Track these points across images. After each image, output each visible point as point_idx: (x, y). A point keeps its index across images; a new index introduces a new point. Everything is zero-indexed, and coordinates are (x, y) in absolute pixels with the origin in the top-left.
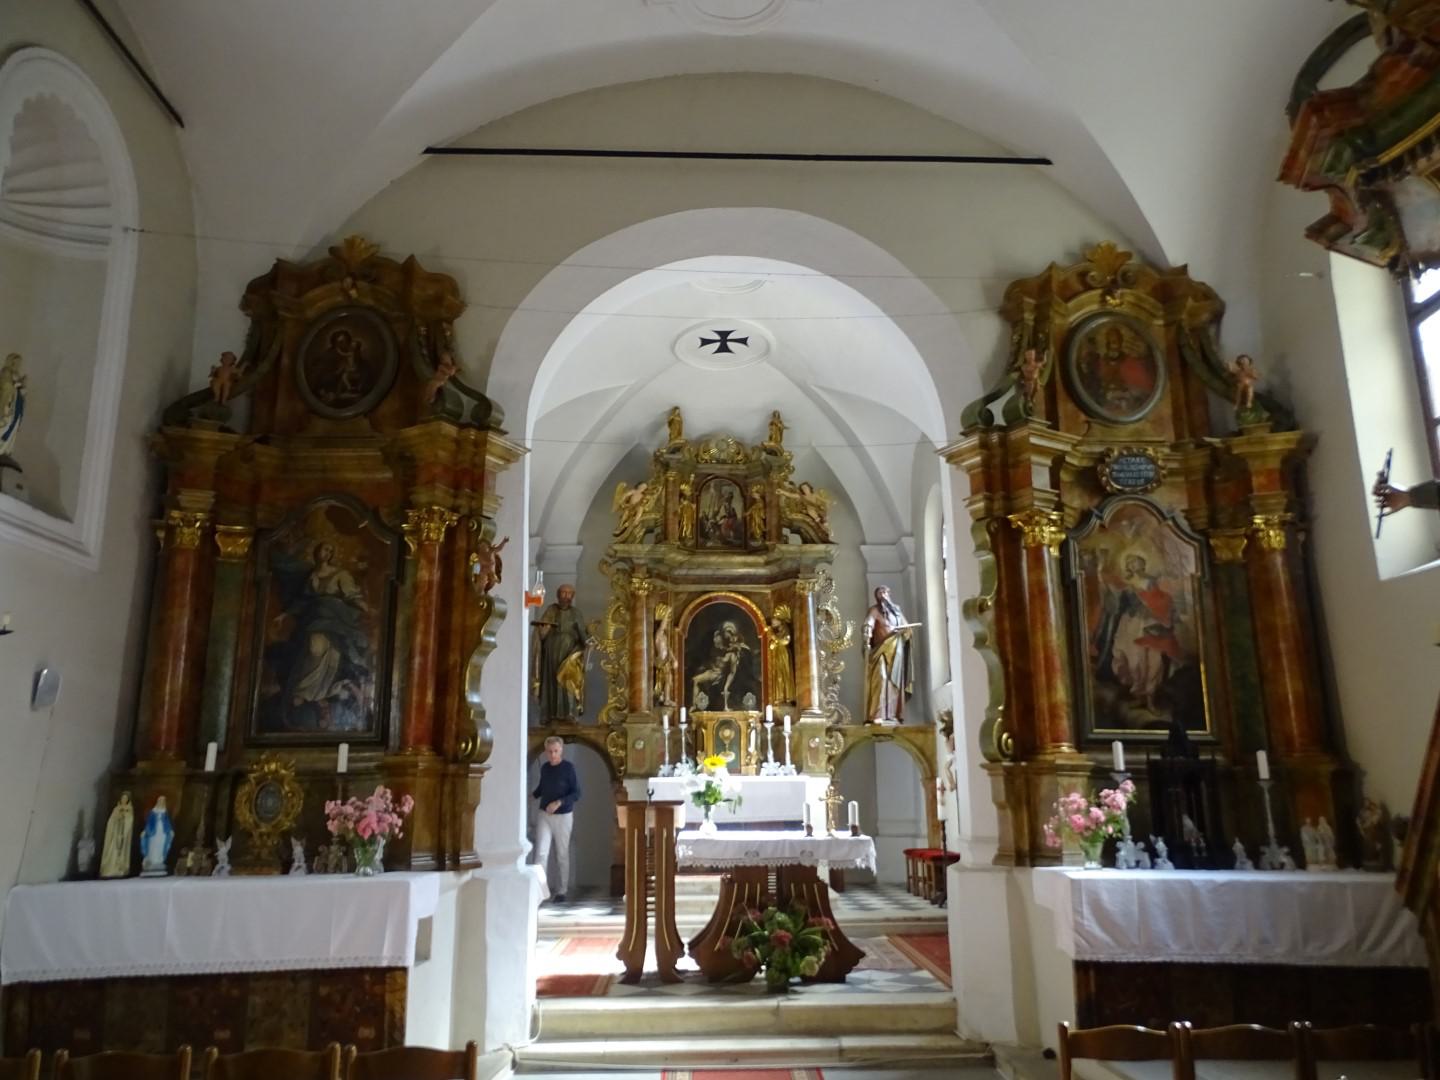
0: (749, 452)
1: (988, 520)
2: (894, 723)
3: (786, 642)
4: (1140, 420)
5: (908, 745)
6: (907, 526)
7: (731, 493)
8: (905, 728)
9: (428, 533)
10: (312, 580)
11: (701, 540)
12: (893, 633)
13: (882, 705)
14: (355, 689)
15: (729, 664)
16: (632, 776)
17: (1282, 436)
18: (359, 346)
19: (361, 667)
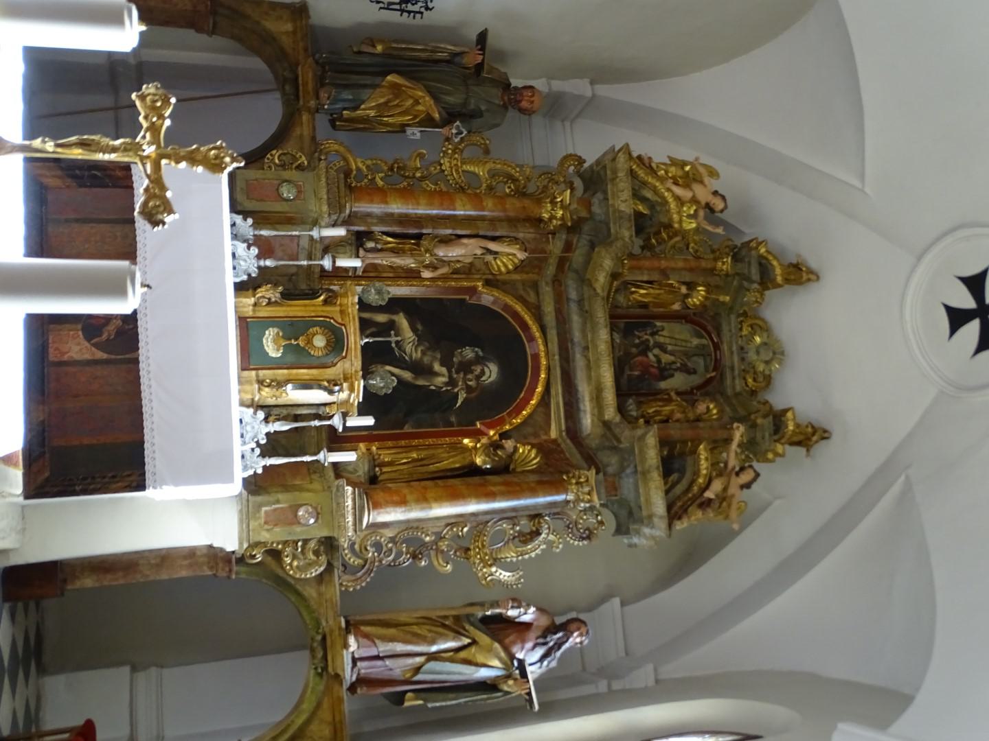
2: (349, 676)
3: (478, 461)
5: (307, 707)
6: (672, 670)
7: (695, 372)
8: (340, 700)
12: (512, 657)
13: (384, 648)
15: (429, 372)
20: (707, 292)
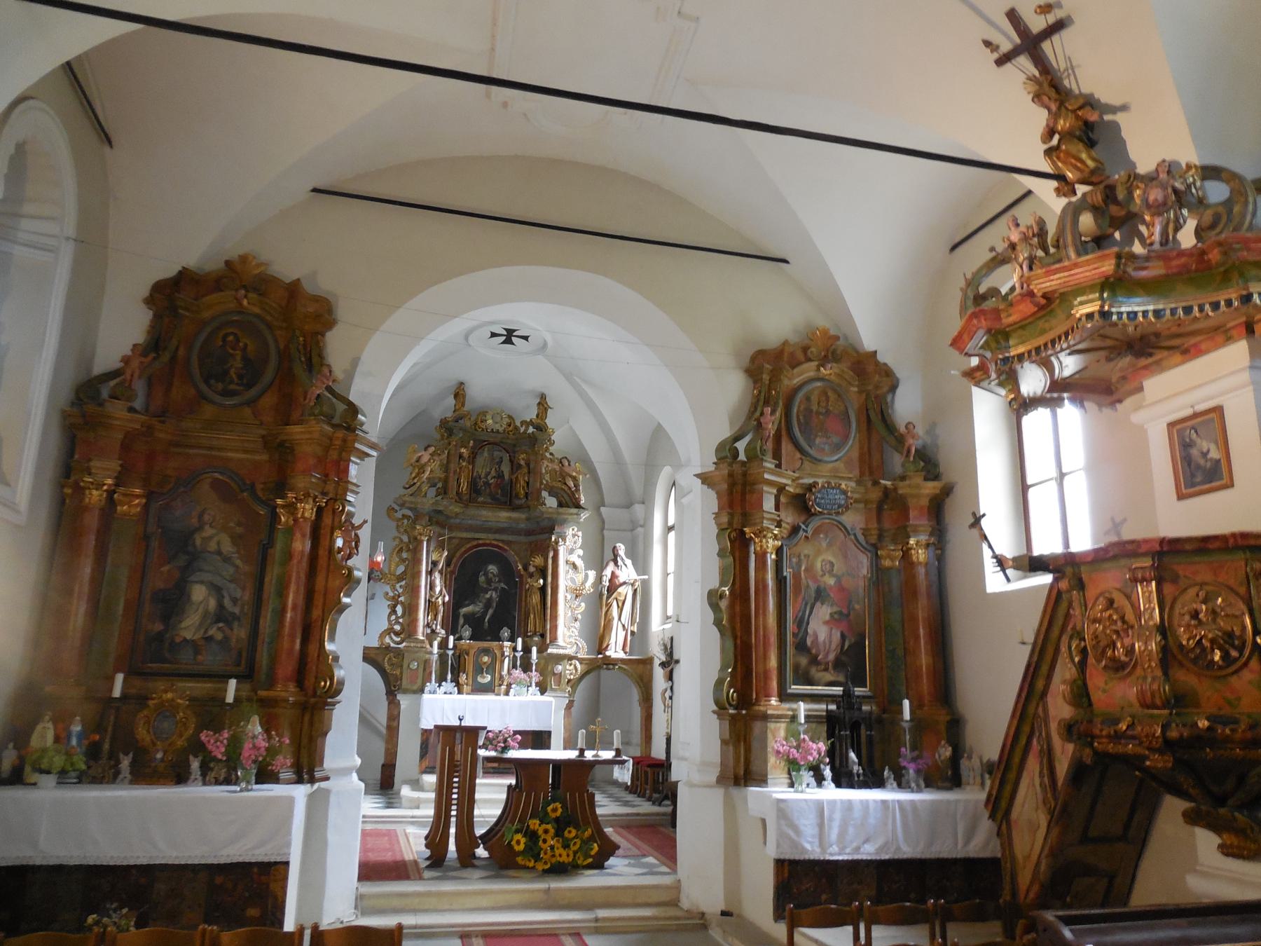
0: (518, 424)
1: (729, 531)
4: (836, 460)
9: (303, 513)
10: (194, 539)
11: (474, 495)
12: (624, 583)
14: (228, 631)
15: (490, 601)
16: (406, 691)
17: (931, 484)
18: (246, 345)
19: (235, 614)
20: (465, 447)
